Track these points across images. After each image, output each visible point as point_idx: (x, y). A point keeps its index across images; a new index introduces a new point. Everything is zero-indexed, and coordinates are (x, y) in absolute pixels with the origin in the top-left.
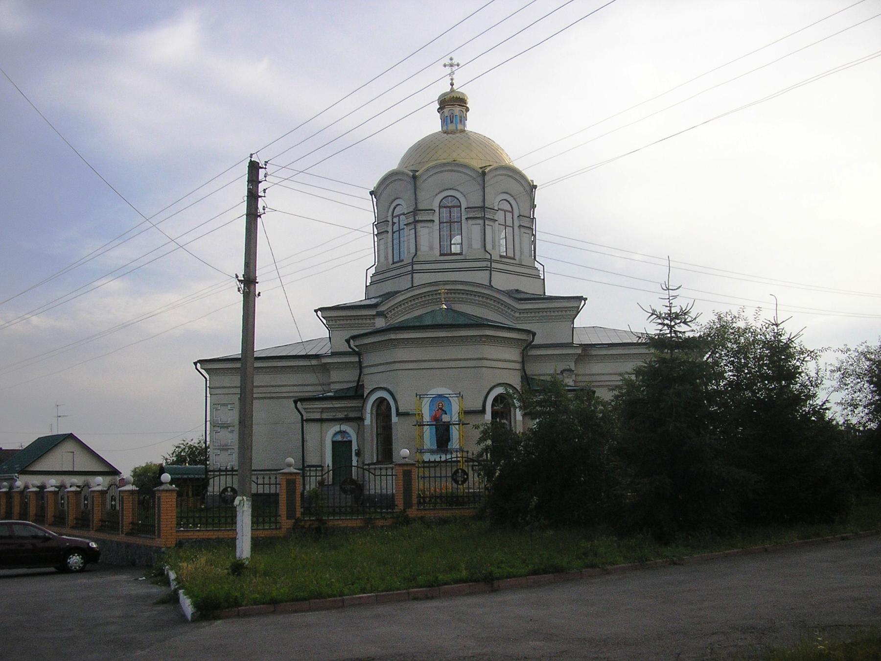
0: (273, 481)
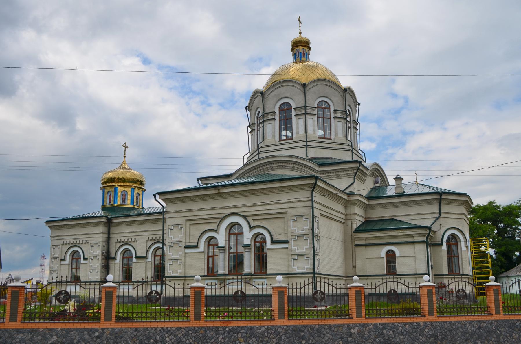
0: (181, 286)
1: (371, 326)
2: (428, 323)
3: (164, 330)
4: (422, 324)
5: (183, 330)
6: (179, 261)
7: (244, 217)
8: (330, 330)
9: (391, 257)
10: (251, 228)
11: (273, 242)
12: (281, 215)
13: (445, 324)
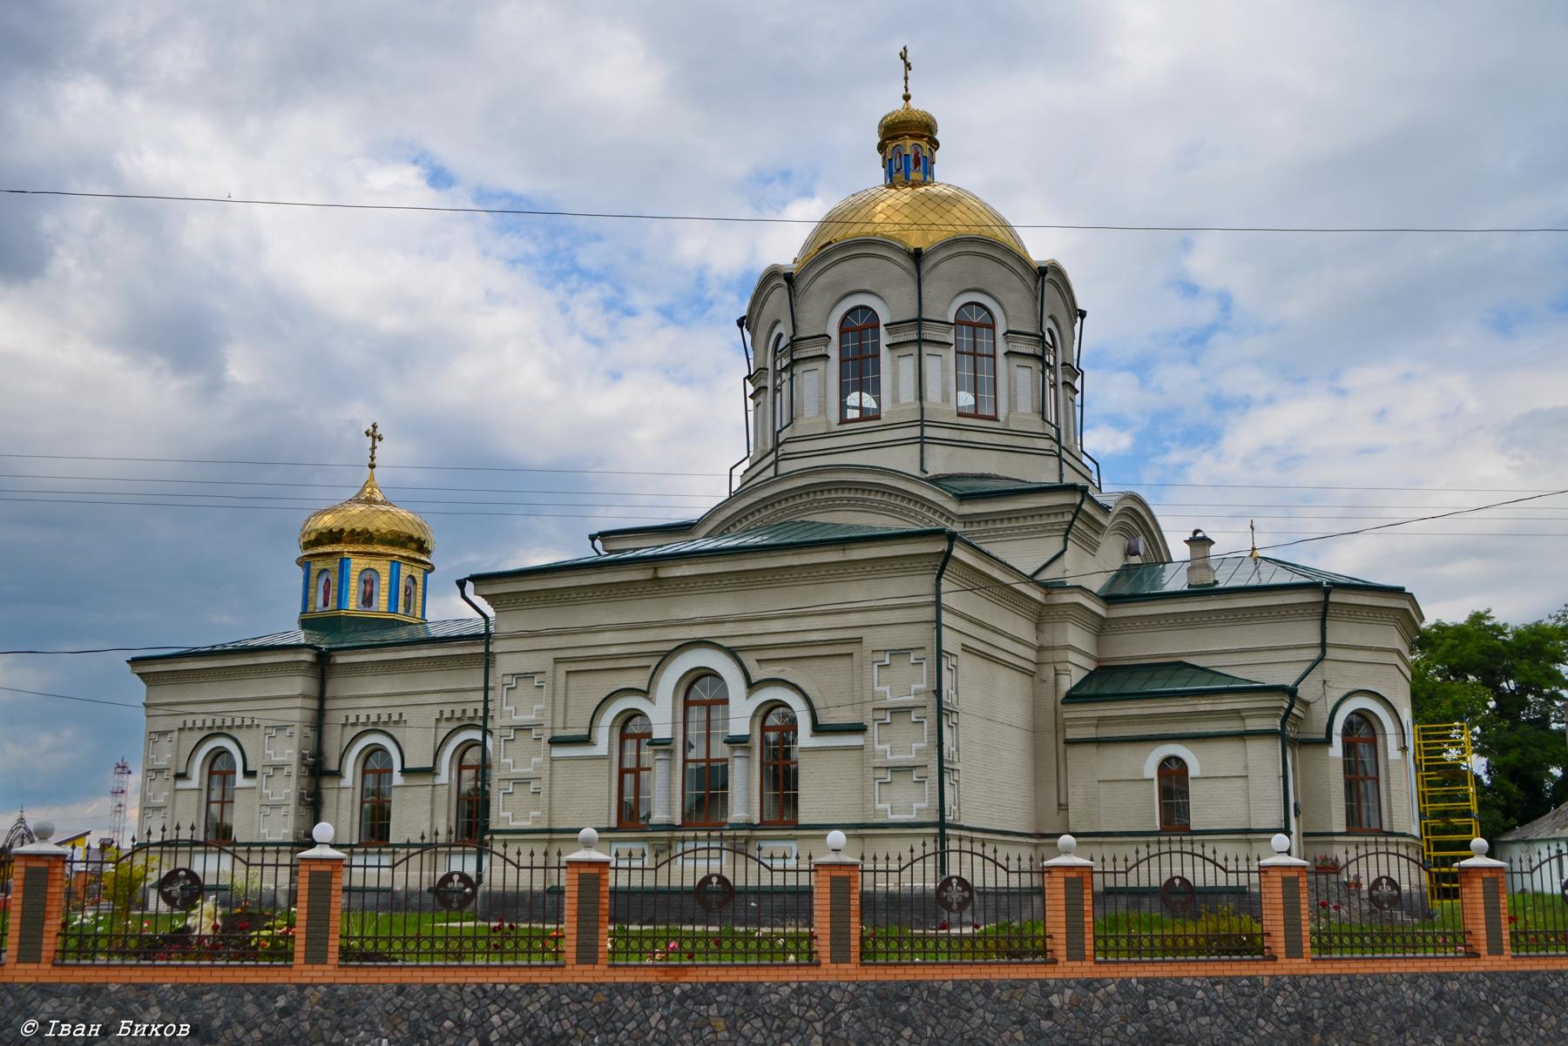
1: (1112, 988)
2: (1286, 979)
3: (485, 992)
5: (542, 992)
7: (732, 652)
8: (987, 997)
10: (752, 686)
11: (818, 729)
12: (843, 648)
13: (1336, 983)
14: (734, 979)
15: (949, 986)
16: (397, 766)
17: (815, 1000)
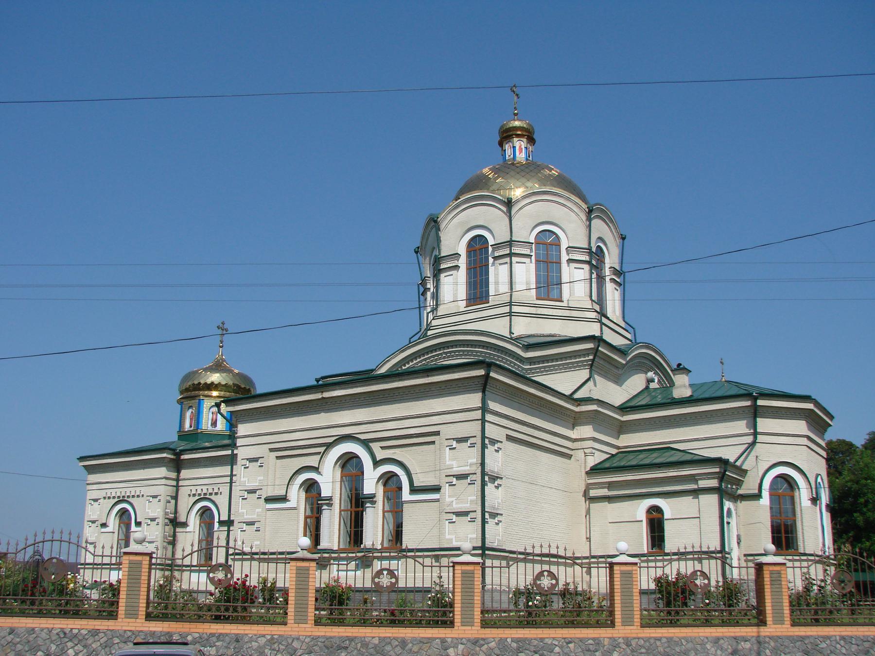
1: (493, 644)
2: (621, 640)
3: (65, 634)
4: (606, 642)
5: (101, 635)
6: (256, 525)
7: (366, 444)
8: (403, 649)
9: (656, 525)
10: (376, 463)
11: (414, 490)
12: (428, 438)
13: (658, 643)
14: (228, 632)
15: (376, 641)
16: (217, 520)
17: (282, 647)
